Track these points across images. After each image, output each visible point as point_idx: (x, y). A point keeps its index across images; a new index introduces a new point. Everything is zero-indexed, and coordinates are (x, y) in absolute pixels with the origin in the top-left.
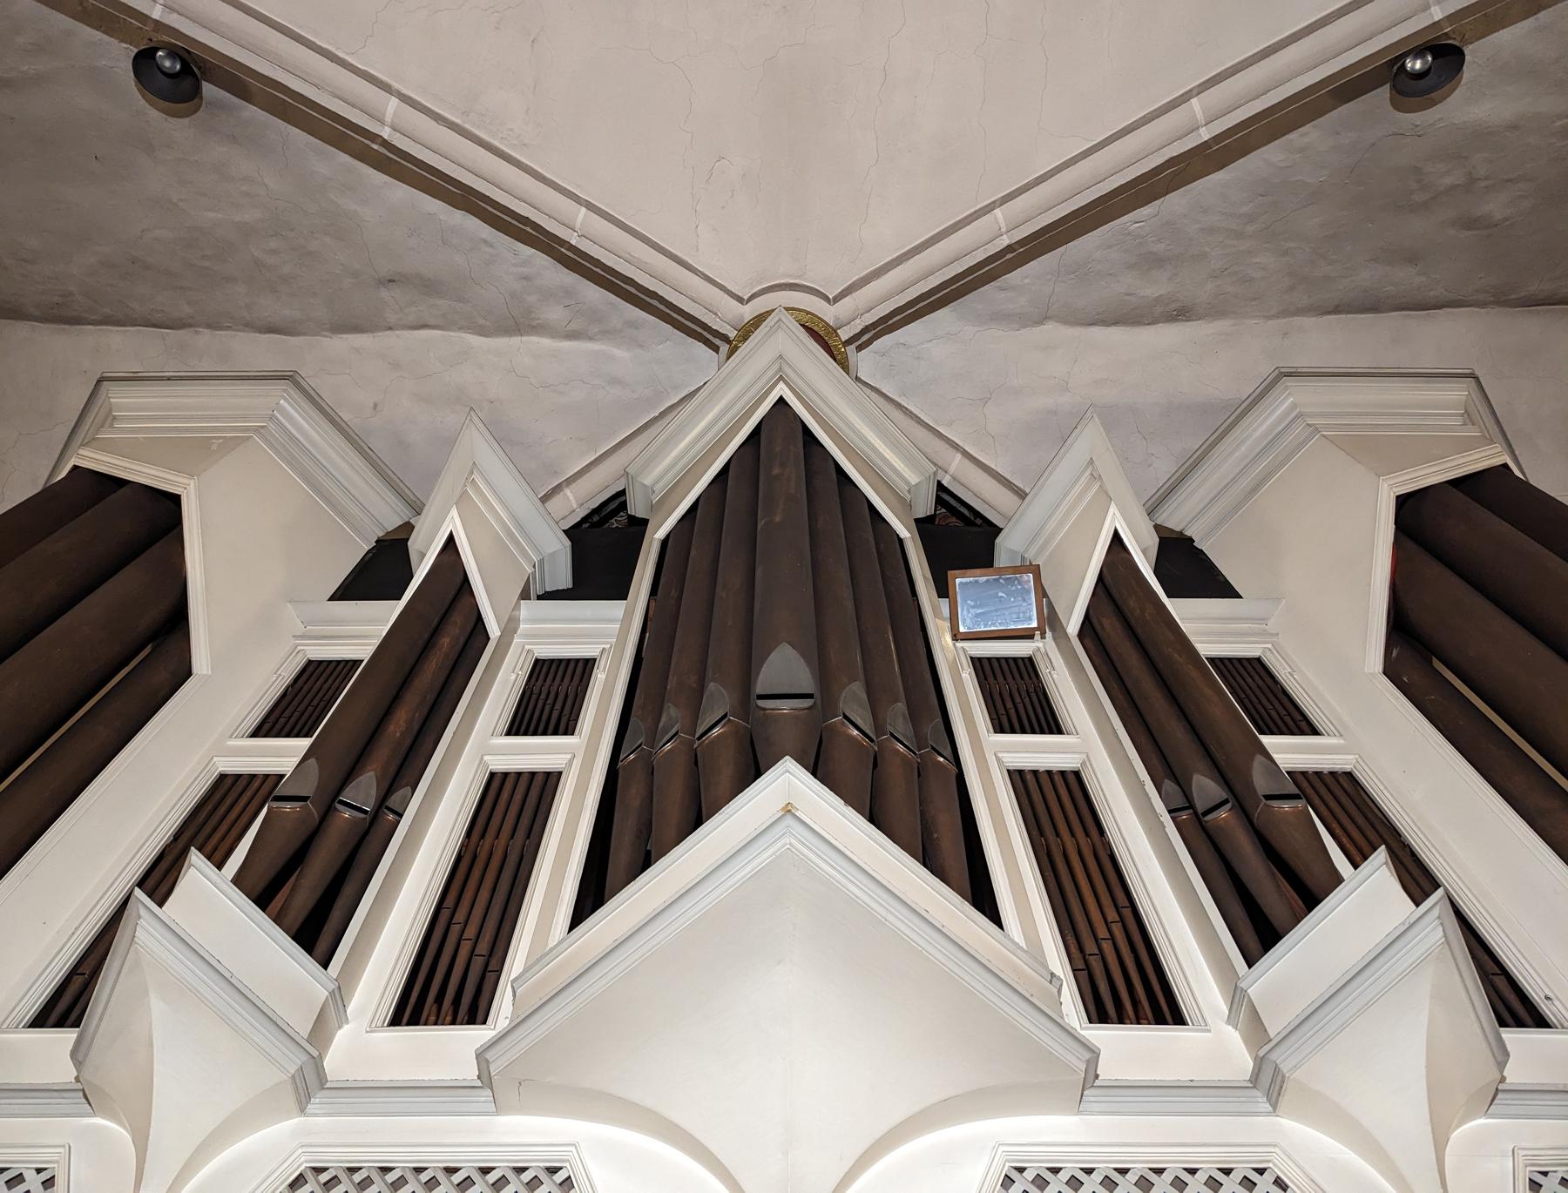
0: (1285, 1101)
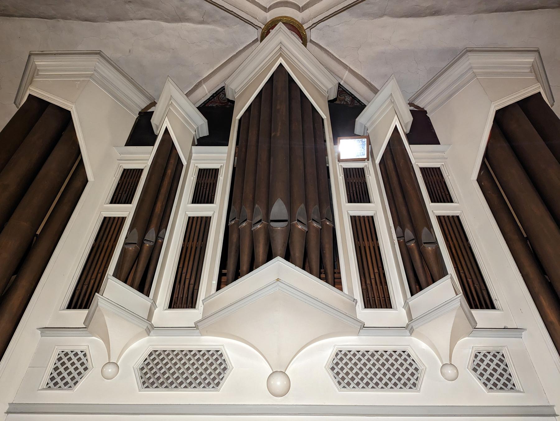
0: (414, 333)
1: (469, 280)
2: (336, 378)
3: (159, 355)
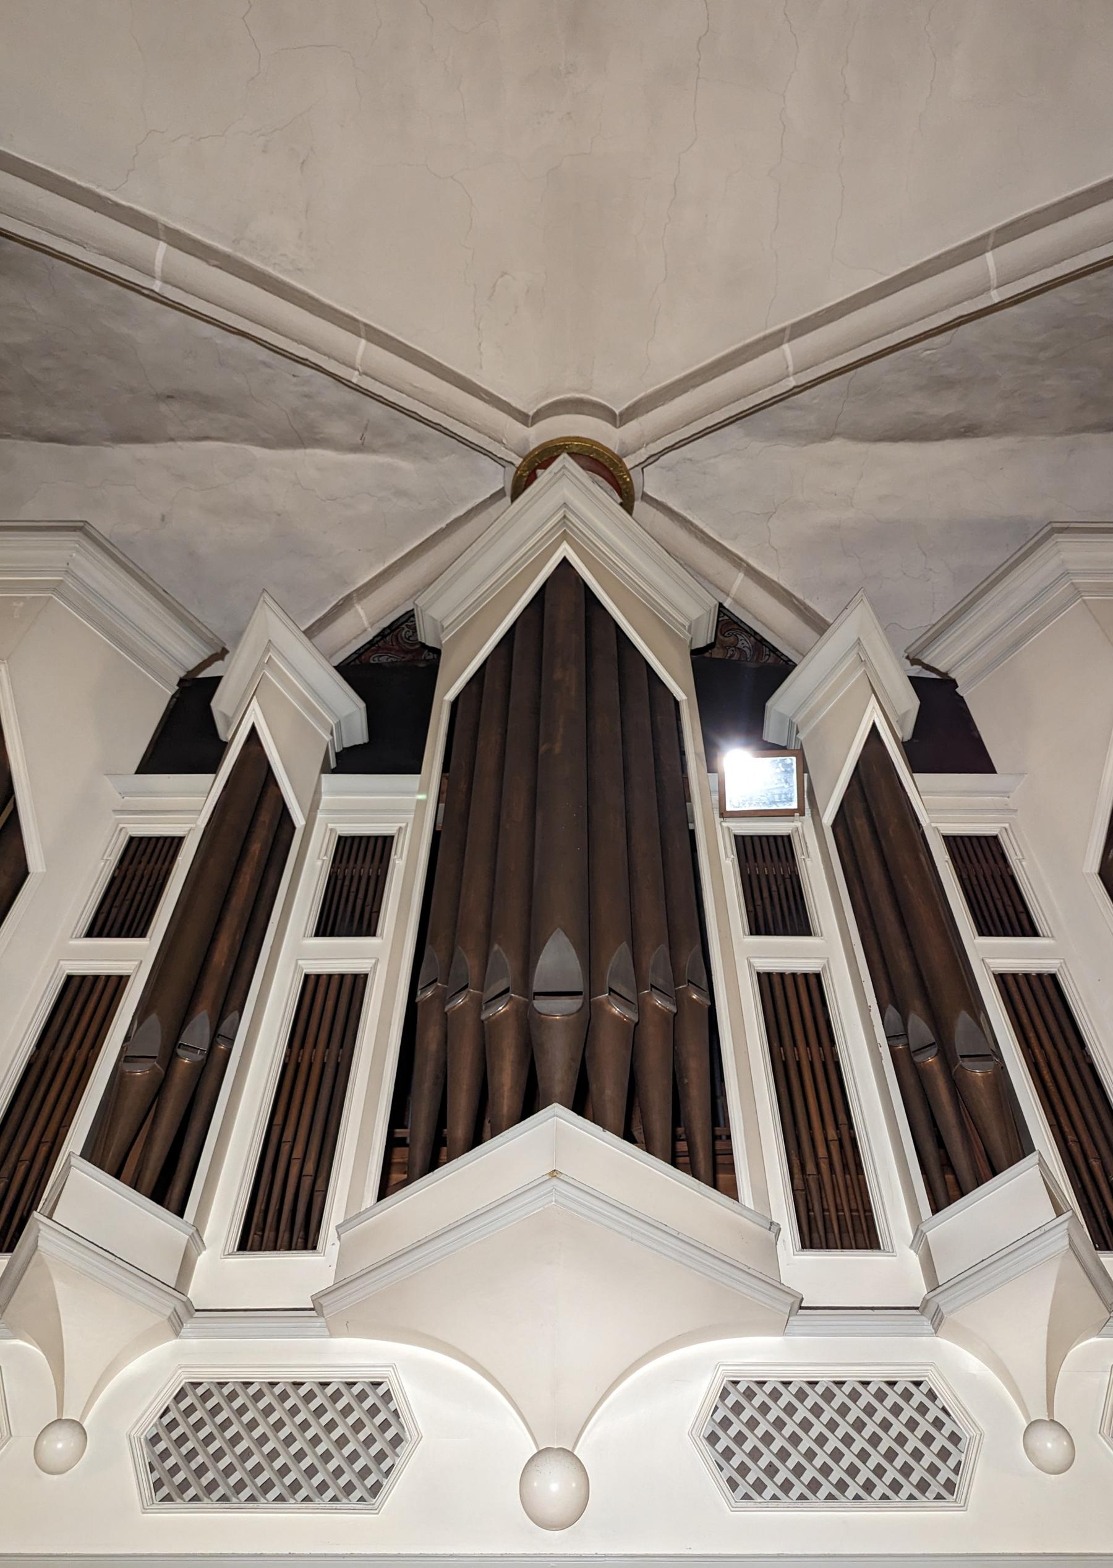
0: (941, 1330)
1: (1094, 1163)
2: (722, 1469)
3: (206, 1396)
